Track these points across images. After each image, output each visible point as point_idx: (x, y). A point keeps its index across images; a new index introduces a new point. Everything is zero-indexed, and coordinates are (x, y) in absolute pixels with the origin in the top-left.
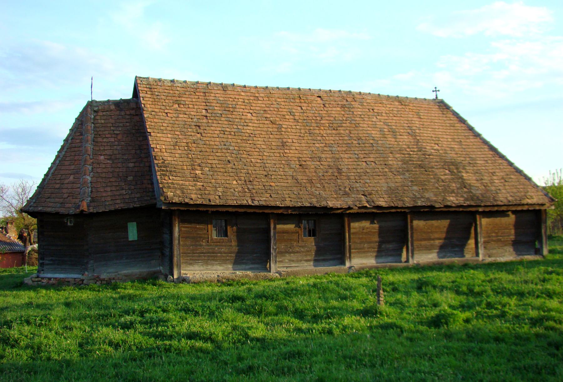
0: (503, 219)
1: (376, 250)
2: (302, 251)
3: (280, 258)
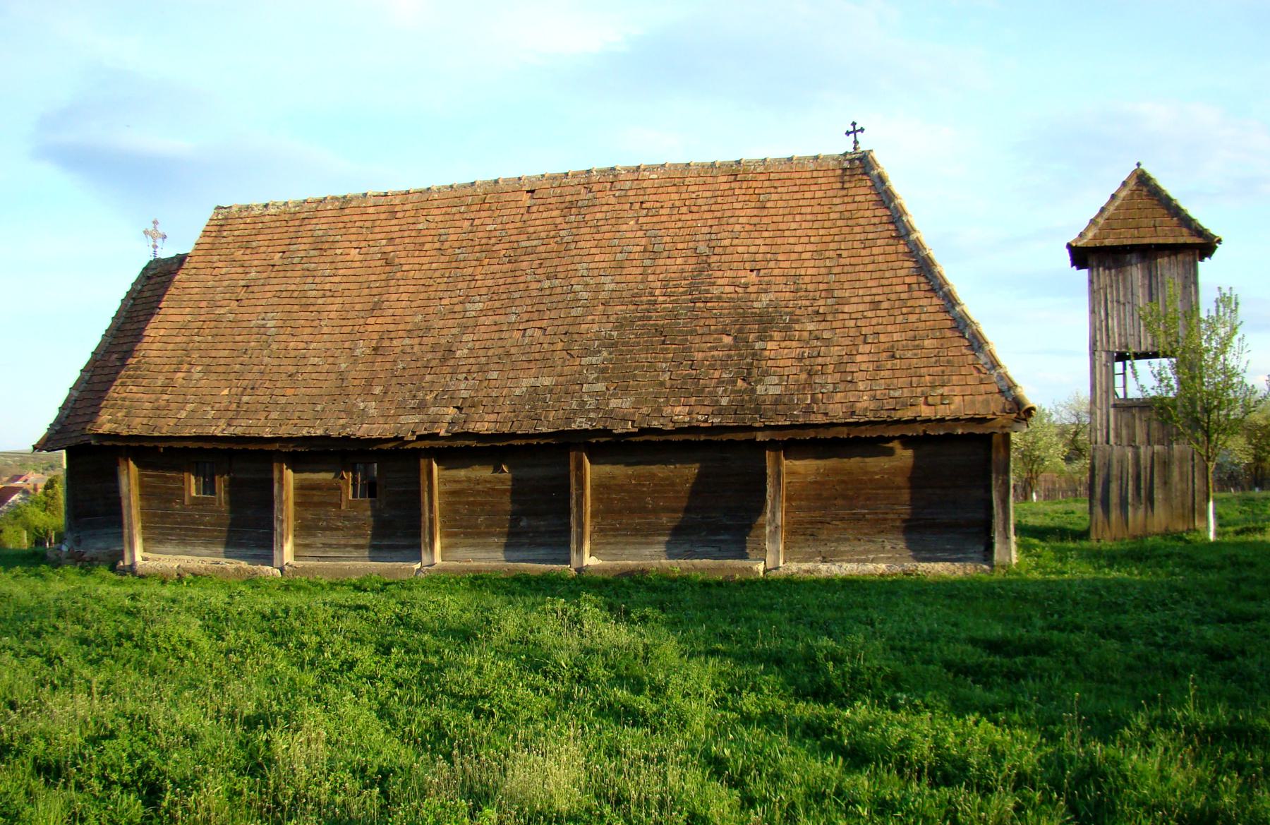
0: (868, 460)
1: (506, 530)
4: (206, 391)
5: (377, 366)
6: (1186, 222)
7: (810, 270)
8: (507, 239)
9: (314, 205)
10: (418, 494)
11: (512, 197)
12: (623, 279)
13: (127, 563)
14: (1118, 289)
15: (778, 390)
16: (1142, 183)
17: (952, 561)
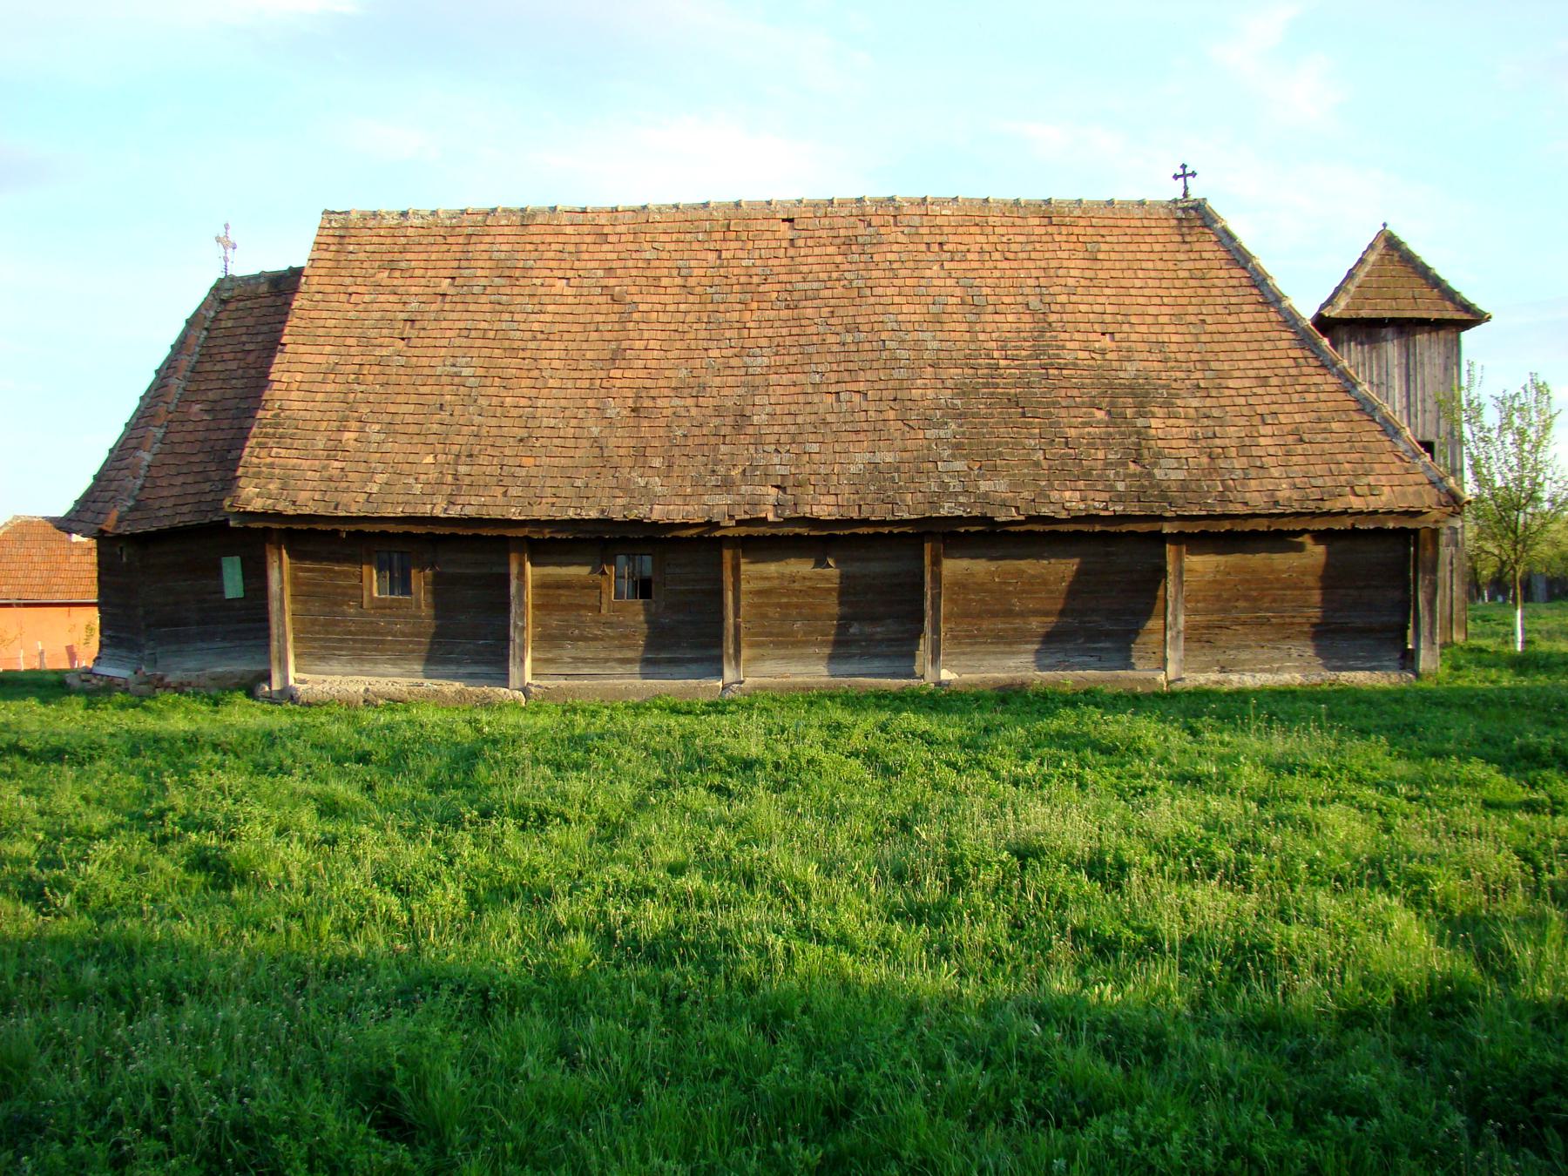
0: (1276, 556)
1: (831, 638)
2: (608, 636)
3: (549, 652)
4: (400, 458)
5: (645, 432)
6: (1449, 295)
7: (1173, 337)
8: (776, 279)
9: (480, 218)
10: (720, 593)
11: (765, 225)
12: (946, 336)
13: (276, 686)
14: (1371, 368)
15: (1181, 475)
16: (1390, 245)
17: (1371, 669)
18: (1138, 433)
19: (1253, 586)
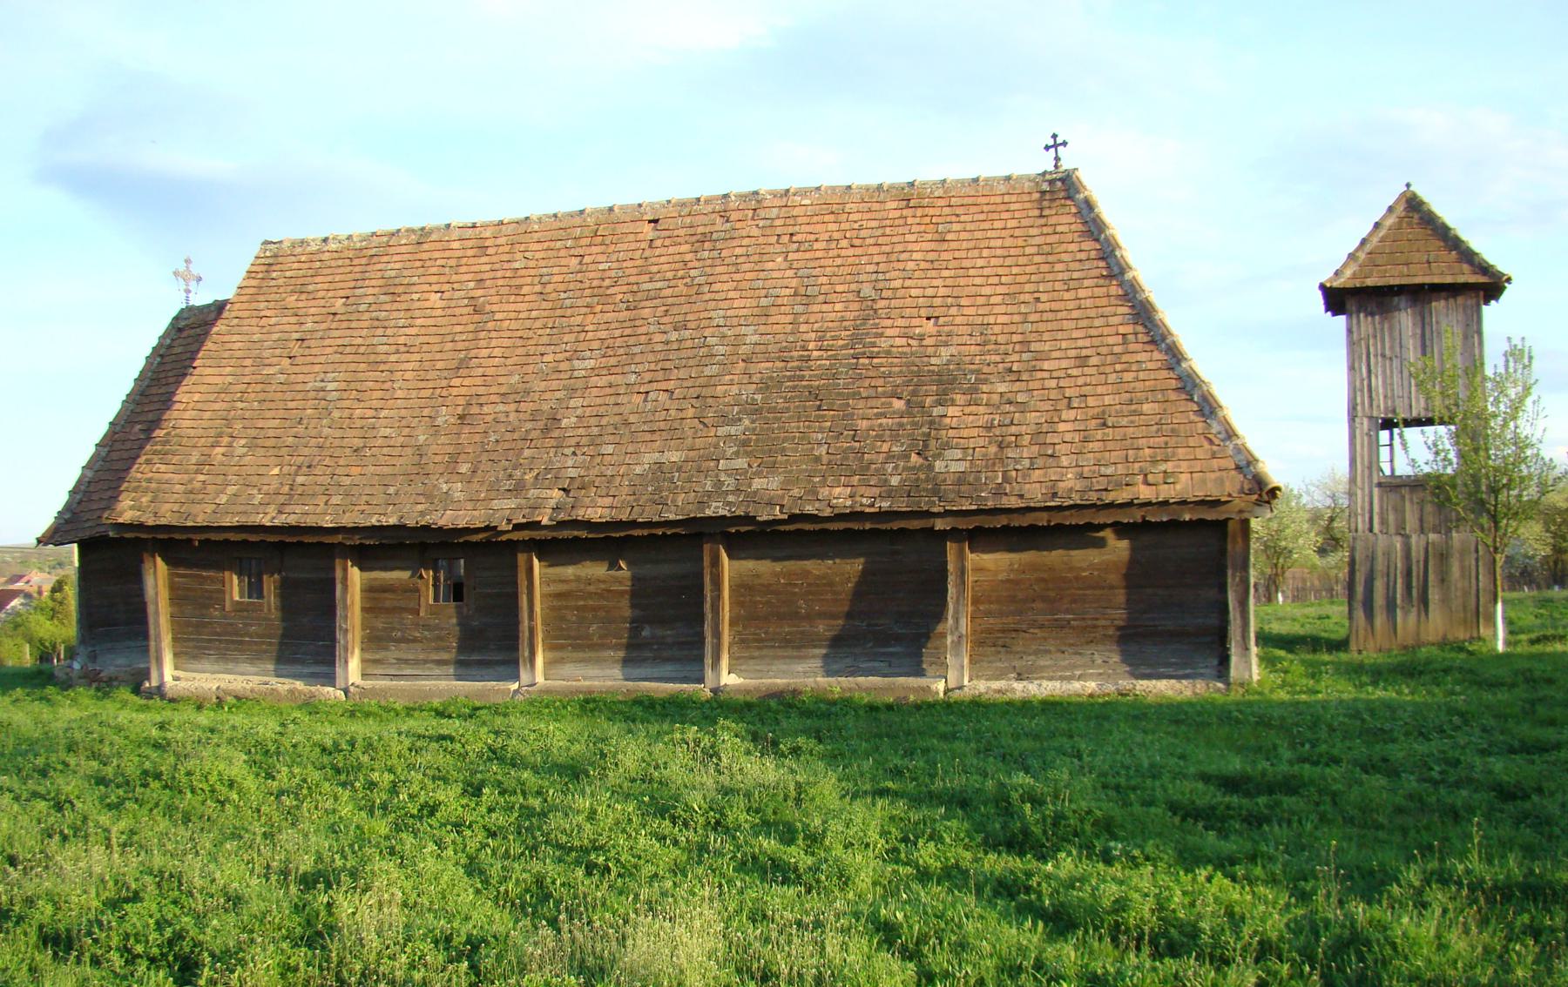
1: (624, 641)
2: (426, 638)
5: (463, 439)
6: (1468, 256)
8: (625, 280)
9: (385, 239)
12: (768, 329)
13: (155, 683)
16: (1413, 206)
17: (1178, 678)
18: (931, 423)
19: (1051, 586)
